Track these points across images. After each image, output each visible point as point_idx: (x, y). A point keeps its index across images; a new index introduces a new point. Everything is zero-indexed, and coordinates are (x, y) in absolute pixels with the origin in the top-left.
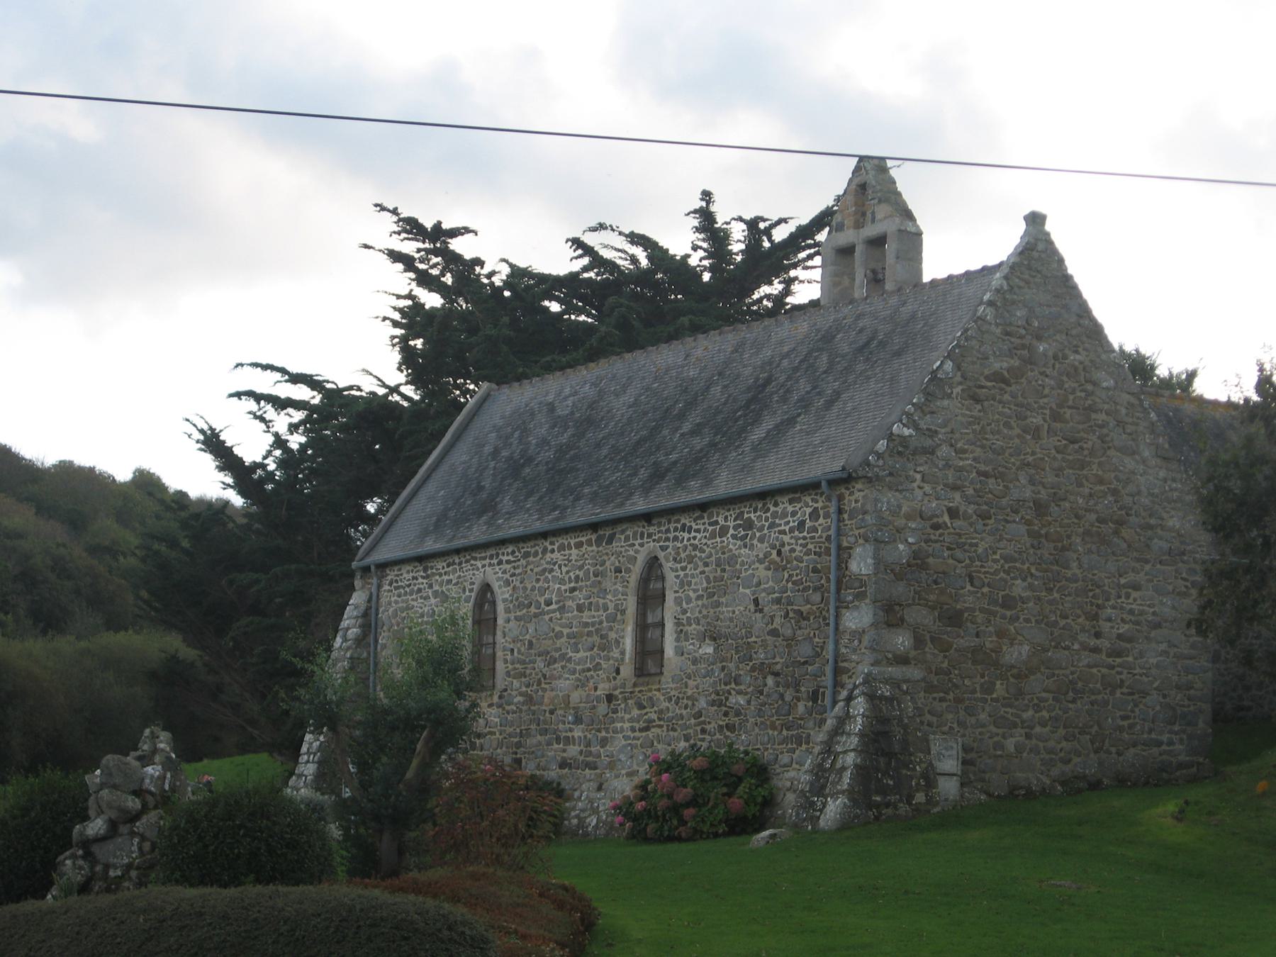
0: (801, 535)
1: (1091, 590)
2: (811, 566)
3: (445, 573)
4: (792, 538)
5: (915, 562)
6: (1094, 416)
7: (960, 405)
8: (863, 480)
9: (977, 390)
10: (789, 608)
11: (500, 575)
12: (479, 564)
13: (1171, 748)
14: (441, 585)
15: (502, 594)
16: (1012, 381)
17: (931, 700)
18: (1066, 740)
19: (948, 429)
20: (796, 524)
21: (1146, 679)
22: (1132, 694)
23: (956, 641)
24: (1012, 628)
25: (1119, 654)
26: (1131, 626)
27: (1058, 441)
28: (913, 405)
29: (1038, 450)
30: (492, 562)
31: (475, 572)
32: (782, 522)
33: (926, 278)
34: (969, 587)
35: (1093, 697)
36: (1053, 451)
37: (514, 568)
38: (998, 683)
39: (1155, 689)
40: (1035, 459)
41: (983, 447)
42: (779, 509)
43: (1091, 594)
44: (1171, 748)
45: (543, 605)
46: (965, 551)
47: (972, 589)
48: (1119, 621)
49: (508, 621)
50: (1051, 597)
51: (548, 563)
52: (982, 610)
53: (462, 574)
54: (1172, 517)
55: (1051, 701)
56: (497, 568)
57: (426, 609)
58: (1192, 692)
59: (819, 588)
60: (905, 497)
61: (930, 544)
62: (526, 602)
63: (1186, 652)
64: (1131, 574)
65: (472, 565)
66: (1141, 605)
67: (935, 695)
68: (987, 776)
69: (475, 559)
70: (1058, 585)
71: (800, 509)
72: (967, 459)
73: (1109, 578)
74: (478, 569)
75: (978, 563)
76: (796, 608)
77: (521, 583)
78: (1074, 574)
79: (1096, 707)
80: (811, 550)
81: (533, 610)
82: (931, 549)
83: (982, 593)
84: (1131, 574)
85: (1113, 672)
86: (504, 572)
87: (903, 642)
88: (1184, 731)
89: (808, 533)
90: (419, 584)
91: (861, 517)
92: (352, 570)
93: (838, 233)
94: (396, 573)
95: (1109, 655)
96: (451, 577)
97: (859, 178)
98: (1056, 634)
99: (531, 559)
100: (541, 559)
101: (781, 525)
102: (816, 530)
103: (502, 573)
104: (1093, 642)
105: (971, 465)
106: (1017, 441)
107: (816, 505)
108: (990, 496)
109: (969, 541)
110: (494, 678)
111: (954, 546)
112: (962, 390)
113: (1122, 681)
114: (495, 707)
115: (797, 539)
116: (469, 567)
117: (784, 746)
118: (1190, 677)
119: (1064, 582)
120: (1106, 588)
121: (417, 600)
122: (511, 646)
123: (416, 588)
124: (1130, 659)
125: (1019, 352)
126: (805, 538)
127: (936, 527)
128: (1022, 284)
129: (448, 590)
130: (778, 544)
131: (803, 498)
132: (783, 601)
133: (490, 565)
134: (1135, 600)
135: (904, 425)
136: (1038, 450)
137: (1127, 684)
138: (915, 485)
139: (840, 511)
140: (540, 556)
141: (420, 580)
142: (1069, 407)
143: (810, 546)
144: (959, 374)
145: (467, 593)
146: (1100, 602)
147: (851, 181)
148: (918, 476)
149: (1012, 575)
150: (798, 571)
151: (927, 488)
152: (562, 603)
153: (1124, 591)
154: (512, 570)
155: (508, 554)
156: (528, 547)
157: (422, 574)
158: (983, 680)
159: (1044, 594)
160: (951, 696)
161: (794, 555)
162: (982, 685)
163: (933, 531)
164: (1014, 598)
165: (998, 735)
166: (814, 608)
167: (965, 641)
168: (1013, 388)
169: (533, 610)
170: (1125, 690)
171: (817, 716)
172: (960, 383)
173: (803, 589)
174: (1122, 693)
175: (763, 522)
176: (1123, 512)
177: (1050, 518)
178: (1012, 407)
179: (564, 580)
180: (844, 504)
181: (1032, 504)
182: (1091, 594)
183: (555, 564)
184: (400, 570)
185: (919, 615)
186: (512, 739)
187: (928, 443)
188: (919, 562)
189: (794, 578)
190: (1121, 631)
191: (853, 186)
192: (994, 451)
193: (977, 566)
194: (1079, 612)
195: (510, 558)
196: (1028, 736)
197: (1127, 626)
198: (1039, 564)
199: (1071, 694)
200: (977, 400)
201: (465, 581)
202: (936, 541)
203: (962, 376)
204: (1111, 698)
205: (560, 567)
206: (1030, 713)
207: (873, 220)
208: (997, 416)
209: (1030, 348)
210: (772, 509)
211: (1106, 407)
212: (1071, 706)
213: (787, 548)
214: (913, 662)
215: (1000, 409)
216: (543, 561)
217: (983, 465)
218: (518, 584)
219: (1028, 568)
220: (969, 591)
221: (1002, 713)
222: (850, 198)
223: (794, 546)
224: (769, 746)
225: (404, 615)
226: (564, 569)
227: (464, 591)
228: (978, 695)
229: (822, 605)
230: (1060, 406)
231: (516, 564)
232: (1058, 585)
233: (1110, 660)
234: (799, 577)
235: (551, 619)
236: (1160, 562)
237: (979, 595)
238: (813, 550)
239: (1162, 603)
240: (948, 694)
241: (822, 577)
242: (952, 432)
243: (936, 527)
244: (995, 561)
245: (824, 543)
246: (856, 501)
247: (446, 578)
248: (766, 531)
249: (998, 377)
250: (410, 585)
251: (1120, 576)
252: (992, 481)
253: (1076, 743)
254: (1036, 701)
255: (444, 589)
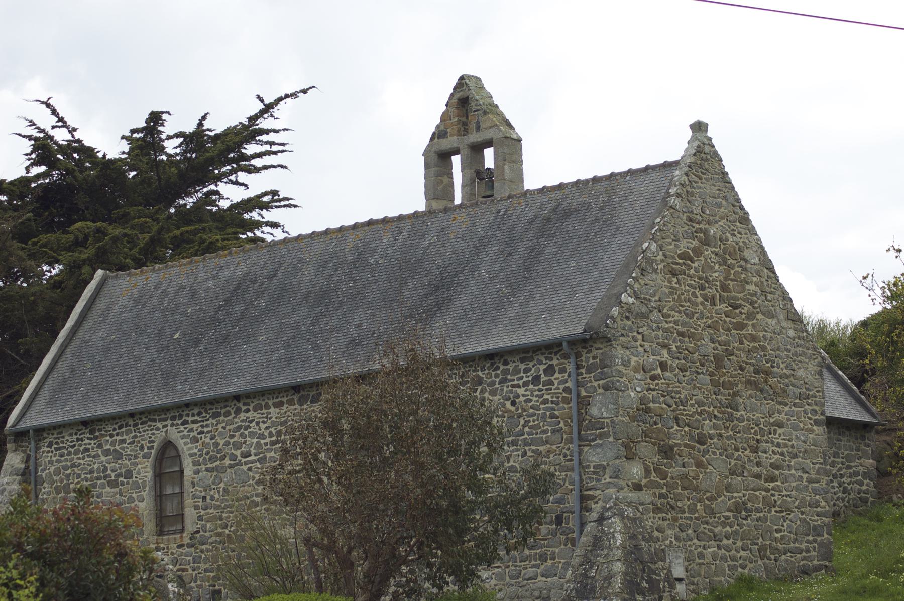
0: (536, 388)
1: (752, 428)
2: (548, 413)
3: (117, 435)
4: (526, 390)
5: (641, 406)
6: (747, 287)
7: (663, 278)
8: (601, 340)
9: (674, 266)
10: (527, 448)
11: (186, 433)
12: (159, 425)
13: (808, 554)
14: (113, 444)
15: (186, 448)
16: (695, 259)
17: (657, 519)
18: (744, 550)
19: (657, 298)
20: (530, 378)
21: (789, 499)
22: (782, 512)
23: (670, 471)
24: (704, 459)
25: (773, 479)
26: (778, 456)
27: (726, 307)
28: (633, 278)
29: (714, 315)
30: (175, 422)
31: (154, 431)
32: (515, 377)
33: (533, 180)
34: (676, 427)
35: (758, 515)
36: (723, 315)
37: (202, 426)
38: (699, 504)
39: (796, 507)
40: (712, 322)
41: (679, 312)
42: (511, 367)
43: (753, 431)
44: (808, 554)
45: (239, 458)
46: (672, 397)
47: (678, 428)
48: (771, 453)
49: (197, 472)
50: (728, 434)
51: (242, 421)
52: (686, 446)
53: (138, 435)
54: (800, 368)
55: (732, 519)
56: (182, 428)
57: (96, 467)
58: (819, 509)
59: (558, 431)
60: (632, 354)
61: (650, 392)
62: (219, 456)
63: (813, 477)
64: (776, 415)
65: (150, 426)
66: (784, 439)
67: (660, 515)
68: (695, 580)
69: (155, 421)
70: (732, 424)
71: (533, 366)
72: (671, 322)
73: (763, 418)
74: (158, 429)
75: (682, 407)
76: (534, 448)
77: (211, 439)
78: (742, 415)
79: (760, 523)
80: (548, 399)
81: (227, 462)
82: (651, 396)
83: (685, 432)
84: (776, 415)
85: (769, 494)
86: (191, 430)
87: (637, 472)
88: (815, 541)
89: (543, 386)
90: (85, 444)
91: (599, 370)
92: (4, 435)
93: (441, 140)
94: (55, 436)
95: (766, 481)
96: (125, 437)
97: (461, 94)
98: (732, 464)
99: (222, 418)
100: (234, 418)
101: (513, 380)
102: (552, 383)
103: (188, 432)
104: (756, 470)
105: (673, 327)
106: (700, 307)
107: (551, 363)
108: (686, 352)
109: (675, 389)
110: (183, 522)
111: (665, 393)
112: (664, 266)
113: (775, 501)
114: (185, 547)
115: (532, 391)
116: (147, 428)
117: (527, 563)
118: (817, 497)
119: (736, 422)
120: (762, 426)
121: (83, 458)
122: (203, 494)
123: (82, 449)
124: (779, 483)
125: (698, 235)
126: (540, 390)
127: (653, 378)
128: (697, 179)
129: (123, 449)
130: (511, 395)
131: (536, 358)
132: (520, 443)
133: (172, 425)
134: (780, 435)
135: (629, 296)
136: (714, 315)
137: (778, 503)
138: (638, 344)
139: (578, 367)
140: (233, 415)
141: (87, 441)
142: (732, 280)
143: (546, 397)
144: (661, 253)
145: (146, 450)
146: (759, 437)
147: (452, 95)
148: (640, 337)
149: (703, 417)
150: (535, 418)
151: (647, 345)
152: (261, 455)
153: (773, 428)
154: (200, 429)
155: (193, 415)
156: (217, 408)
157: (88, 435)
158: (689, 503)
159: (723, 432)
160: (670, 516)
161: (530, 404)
162: (688, 506)
163: (651, 382)
164: (704, 435)
165: (700, 546)
166: (554, 447)
167: (675, 471)
168: (696, 264)
169: (227, 462)
170: (778, 509)
171: (562, 537)
172: (662, 261)
173: (541, 432)
174: (776, 511)
175: (493, 378)
176: (769, 365)
177: (724, 370)
178: (696, 279)
179: (263, 435)
180: (582, 361)
181: (712, 359)
182: (753, 431)
183: (251, 422)
184: (61, 433)
185: (646, 450)
186: (208, 574)
187: (644, 310)
188: (644, 406)
189: (531, 424)
190: (772, 461)
191: (455, 101)
192: (687, 315)
193: (680, 410)
194: (745, 445)
195: (196, 418)
196: (719, 547)
197: (776, 457)
198: (720, 408)
199: (744, 513)
200: (674, 274)
201: (142, 440)
202: (654, 390)
203: (664, 255)
204: (769, 515)
205: (258, 424)
206: (719, 528)
207: (478, 128)
208: (687, 288)
209: (705, 232)
210: (502, 367)
211: (755, 279)
212: (745, 522)
213: (522, 399)
214: (645, 489)
215: (689, 282)
216: (236, 420)
217: (680, 327)
218: (208, 440)
219: (713, 411)
220: (676, 430)
221: (702, 528)
222: (454, 111)
223: (529, 397)
224: (510, 564)
225: (69, 472)
226: (263, 426)
227: (142, 448)
228: (686, 515)
229: (562, 445)
230: (726, 279)
231: (205, 423)
232: (732, 424)
233: (767, 484)
234: (536, 422)
235: (250, 469)
236: (794, 405)
237: (683, 433)
238: (550, 399)
239: (797, 438)
240: (668, 514)
241: (560, 422)
242: (660, 301)
243: (653, 378)
244: (692, 405)
245: (562, 393)
246: (594, 358)
247: (118, 438)
248: (497, 386)
249: (684, 256)
250: (74, 446)
251: (770, 416)
252: (686, 339)
253: (748, 552)
254: (723, 519)
255: (117, 448)
